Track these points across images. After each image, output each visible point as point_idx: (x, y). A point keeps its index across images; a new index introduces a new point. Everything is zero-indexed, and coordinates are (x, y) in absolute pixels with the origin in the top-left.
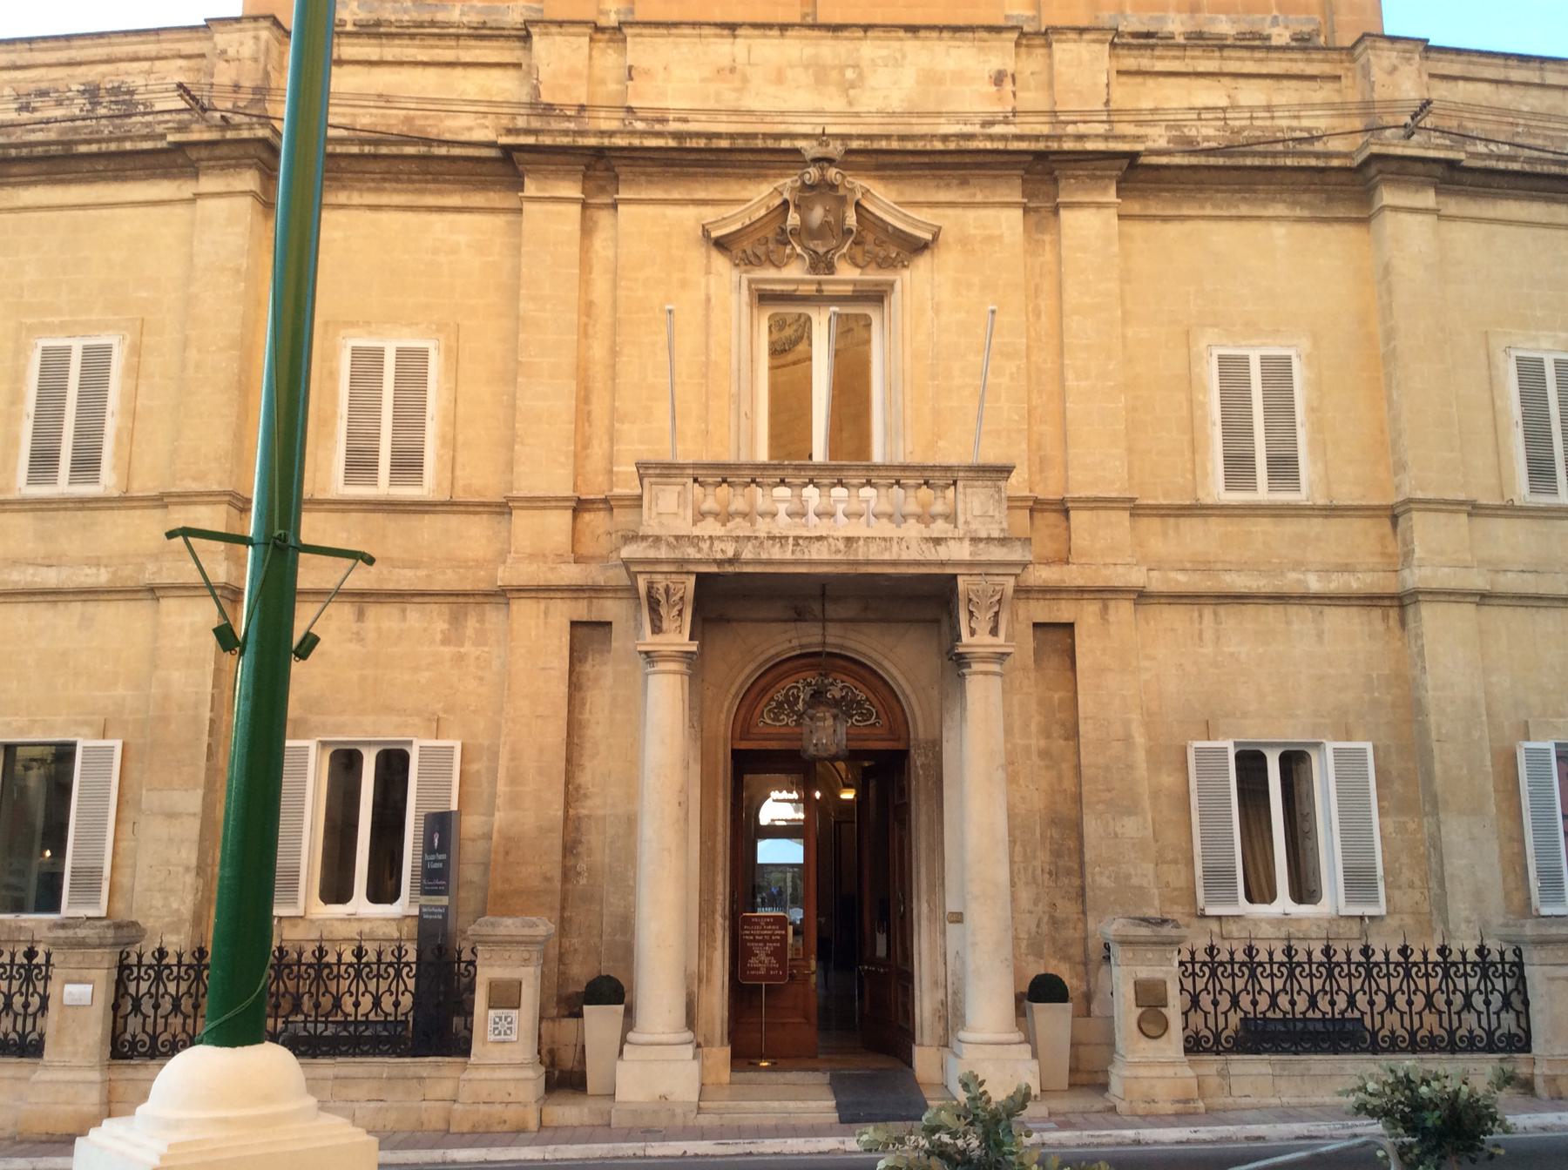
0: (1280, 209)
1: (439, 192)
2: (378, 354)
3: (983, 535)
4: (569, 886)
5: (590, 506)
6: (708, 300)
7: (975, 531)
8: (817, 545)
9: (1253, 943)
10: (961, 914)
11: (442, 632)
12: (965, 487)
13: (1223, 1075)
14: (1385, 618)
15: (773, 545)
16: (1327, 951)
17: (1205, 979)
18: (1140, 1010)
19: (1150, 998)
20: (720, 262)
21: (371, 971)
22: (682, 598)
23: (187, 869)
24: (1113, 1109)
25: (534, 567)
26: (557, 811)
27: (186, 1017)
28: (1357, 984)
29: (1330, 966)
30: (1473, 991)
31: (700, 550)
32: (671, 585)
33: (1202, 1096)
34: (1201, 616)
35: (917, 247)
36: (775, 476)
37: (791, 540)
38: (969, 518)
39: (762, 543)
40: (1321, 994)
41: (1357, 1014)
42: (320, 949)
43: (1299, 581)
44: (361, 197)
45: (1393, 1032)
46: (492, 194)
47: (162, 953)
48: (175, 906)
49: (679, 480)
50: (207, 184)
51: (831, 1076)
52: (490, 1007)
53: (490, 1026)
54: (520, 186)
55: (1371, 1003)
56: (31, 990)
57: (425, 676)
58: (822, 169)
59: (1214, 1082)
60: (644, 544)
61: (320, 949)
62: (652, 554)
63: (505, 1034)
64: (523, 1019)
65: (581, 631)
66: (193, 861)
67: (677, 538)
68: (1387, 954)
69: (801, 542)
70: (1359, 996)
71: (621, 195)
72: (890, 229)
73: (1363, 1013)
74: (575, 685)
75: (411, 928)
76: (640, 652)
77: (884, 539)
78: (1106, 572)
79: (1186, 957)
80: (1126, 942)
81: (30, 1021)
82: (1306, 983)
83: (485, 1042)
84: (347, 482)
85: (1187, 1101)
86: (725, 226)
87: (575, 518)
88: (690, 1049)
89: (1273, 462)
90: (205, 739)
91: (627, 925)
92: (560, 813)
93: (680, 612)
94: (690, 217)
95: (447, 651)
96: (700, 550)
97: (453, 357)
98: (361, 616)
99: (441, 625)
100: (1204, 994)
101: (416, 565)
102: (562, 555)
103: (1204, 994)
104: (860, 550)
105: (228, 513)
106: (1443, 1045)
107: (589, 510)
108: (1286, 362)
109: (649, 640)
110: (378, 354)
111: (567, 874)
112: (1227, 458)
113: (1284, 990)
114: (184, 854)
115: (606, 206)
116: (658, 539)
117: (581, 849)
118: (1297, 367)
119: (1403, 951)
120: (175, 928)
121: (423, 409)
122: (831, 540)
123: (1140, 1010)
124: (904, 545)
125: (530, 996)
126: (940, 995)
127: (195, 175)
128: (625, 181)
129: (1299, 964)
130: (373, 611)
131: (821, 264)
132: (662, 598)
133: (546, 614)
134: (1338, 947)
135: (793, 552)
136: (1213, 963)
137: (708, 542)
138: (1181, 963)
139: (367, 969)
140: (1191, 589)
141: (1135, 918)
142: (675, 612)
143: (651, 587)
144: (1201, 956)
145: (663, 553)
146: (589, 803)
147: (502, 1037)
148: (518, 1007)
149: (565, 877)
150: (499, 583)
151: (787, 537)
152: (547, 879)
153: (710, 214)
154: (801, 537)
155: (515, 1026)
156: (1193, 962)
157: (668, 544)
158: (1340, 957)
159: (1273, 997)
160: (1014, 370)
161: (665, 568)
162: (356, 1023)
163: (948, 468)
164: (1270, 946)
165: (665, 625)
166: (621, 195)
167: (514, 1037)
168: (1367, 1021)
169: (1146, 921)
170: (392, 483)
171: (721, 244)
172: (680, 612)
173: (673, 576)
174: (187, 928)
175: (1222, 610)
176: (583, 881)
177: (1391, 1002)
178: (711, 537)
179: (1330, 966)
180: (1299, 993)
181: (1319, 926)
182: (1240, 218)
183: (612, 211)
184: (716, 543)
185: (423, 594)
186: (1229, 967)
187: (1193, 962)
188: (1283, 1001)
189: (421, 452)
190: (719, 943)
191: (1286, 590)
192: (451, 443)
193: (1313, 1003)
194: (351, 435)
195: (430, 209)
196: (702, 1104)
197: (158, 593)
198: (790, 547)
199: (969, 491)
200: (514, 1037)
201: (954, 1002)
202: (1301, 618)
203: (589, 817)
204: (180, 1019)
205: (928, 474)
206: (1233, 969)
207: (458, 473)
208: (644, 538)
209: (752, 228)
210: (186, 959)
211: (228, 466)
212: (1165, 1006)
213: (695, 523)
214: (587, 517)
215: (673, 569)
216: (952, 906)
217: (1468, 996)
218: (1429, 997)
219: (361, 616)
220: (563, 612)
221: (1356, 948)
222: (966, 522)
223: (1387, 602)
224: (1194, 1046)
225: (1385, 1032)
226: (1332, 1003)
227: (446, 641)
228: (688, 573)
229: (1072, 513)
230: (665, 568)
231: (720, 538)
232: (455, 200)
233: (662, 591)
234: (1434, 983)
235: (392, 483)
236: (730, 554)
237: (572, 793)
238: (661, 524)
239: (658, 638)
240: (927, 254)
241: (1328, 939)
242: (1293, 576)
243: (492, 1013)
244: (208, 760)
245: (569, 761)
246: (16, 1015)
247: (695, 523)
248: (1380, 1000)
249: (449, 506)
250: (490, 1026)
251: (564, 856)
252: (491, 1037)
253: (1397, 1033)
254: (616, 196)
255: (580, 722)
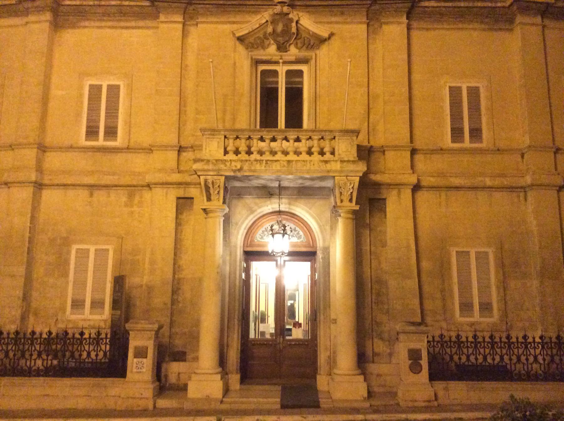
0: (476, 25)
1: (127, 21)
2: (99, 87)
3: (346, 159)
4: (175, 307)
5: (185, 150)
6: (235, 64)
7: (343, 158)
8: (275, 163)
9: (460, 333)
10: (336, 320)
11: (124, 201)
12: (339, 139)
13: (446, 389)
14: (519, 197)
15: (257, 163)
16: (491, 337)
17: (540, 350)
18: (410, 362)
19: (414, 355)
20: (241, 48)
21: (54, 342)
22: (219, 186)
23: (19, 298)
24: (398, 404)
25: (161, 175)
26: (170, 275)
27: (43, 360)
28: (504, 351)
29: (493, 343)
30: (504, 355)
31: (226, 166)
32: (214, 181)
33: (436, 399)
34: (440, 196)
35: (322, 41)
36: (258, 135)
37: (264, 162)
38: (340, 152)
39: (252, 163)
40: (489, 355)
41: (504, 364)
42: (99, 332)
43: (481, 181)
44: (94, 23)
45: (520, 372)
46: (147, 21)
47: (33, 333)
48: (13, 313)
49: (218, 136)
50: (32, 18)
51: (284, 389)
52: (135, 357)
53: (135, 365)
54: (157, 17)
55: (511, 359)
56: (99, 349)
57: (117, 220)
58: (282, 7)
59: (441, 394)
60: (203, 163)
61: (99, 332)
62: (206, 167)
63: (141, 368)
64: (148, 363)
65: (181, 201)
66: (21, 295)
67: (217, 160)
68: (517, 338)
69: (268, 162)
70: (505, 357)
71: (199, 20)
72: (311, 33)
73: (507, 364)
74: (178, 224)
75: (109, 323)
76: (202, 209)
77: (304, 161)
78: (400, 177)
79: (431, 339)
80: (404, 332)
81: (33, 362)
82: (482, 351)
83: (132, 372)
84: (86, 140)
85: (429, 401)
86: (242, 31)
87: (179, 155)
88: (219, 376)
89: (472, 131)
90: (27, 245)
91: (197, 323)
92: (171, 277)
93: (219, 192)
94: (227, 28)
95: (126, 210)
96: (226, 166)
97: (130, 88)
98: (91, 195)
99: (124, 199)
100: (539, 356)
101: (114, 174)
102: (173, 170)
103: (539, 356)
104: (293, 166)
105: (37, 153)
106: (541, 378)
107: (184, 151)
108: (477, 89)
109: (207, 205)
110: (99, 87)
111: (173, 302)
112: (452, 129)
113: (473, 353)
114: (18, 292)
115: (193, 25)
116: (208, 161)
117: (180, 292)
118: (482, 90)
119: (525, 337)
120: (13, 322)
121: (117, 110)
122: (281, 161)
123: (410, 362)
124: (312, 163)
125: (151, 353)
126: (328, 354)
127: (27, 15)
128: (201, 14)
129: (479, 342)
130: (96, 193)
131: (282, 48)
132: (211, 186)
133: (167, 194)
134: (497, 335)
135: (265, 167)
136: (442, 341)
137: (229, 162)
138: (428, 342)
139: (52, 341)
140: (436, 185)
141: (409, 322)
142: (216, 192)
143: (206, 181)
144: (437, 339)
145: (211, 167)
146: (184, 273)
147: (139, 370)
148: (146, 357)
149: (173, 304)
150: (147, 181)
151: (263, 160)
152: (165, 304)
153: (235, 26)
154: (268, 160)
155: (145, 365)
156: (434, 341)
157: (213, 163)
158: (497, 340)
159: (468, 357)
160: (363, 92)
161: (211, 173)
162: (96, 363)
163: (331, 131)
164: (467, 334)
165: (212, 198)
166: (199, 20)
167: (144, 370)
168: (508, 367)
169: (413, 324)
170: (105, 140)
171: (241, 39)
172: (219, 192)
173: (215, 177)
174: (18, 322)
175: (449, 193)
176: (180, 305)
177: (519, 359)
178: (231, 160)
179: (493, 343)
180: (546, 355)
181: (488, 326)
182: (459, 29)
183: (196, 27)
184: (233, 163)
185: (116, 186)
186: (483, 344)
187: (434, 341)
188: (472, 358)
189: (116, 127)
190: (236, 332)
191: (476, 185)
192: (129, 124)
193: (485, 358)
194: (88, 120)
195: (123, 28)
196: (224, 399)
197: (9, 185)
198: (264, 164)
199: (340, 141)
200: (144, 370)
201: (334, 357)
202: (482, 196)
203: (184, 278)
204: (24, 361)
205: (323, 133)
206: (434, 344)
207: (131, 136)
208: (202, 160)
209: (252, 33)
210: (12, 336)
211: (37, 133)
212: (421, 360)
213: (225, 155)
214: (184, 154)
215: (215, 173)
216: (333, 316)
217: (535, 357)
218: (535, 357)
219: (91, 195)
220: (173, 194)
221: (504, 335)
222: (339, 155)
223: (519, 190)
224: (433, 377)
225: (517, 372)
226: (494, 359)
227: (126, 205)
228: (221, 175)
229: (386, 153)
230: (211, 173)
231: (234, 161)
232: (133, 24)
233: (211, 183)
234: (538, 351)
235: (105, 140)
236: (239, 167)
237: (176, 267)
238: (211, 155)
239: (209, 203)
240: (326, 43)
241: (492, 331)
242: (480, 179)
243: (135, 360)
244: (28, 253)
245: (175, 254)
246: (27, 360)
247: (225, 155)
248: (514, 358)
249: (128, 149)
250: (135, 365)
251: (173, 295)
252: (135, 370)
253: (521, 373)
254: (197, 20)
255: (180, 239)
